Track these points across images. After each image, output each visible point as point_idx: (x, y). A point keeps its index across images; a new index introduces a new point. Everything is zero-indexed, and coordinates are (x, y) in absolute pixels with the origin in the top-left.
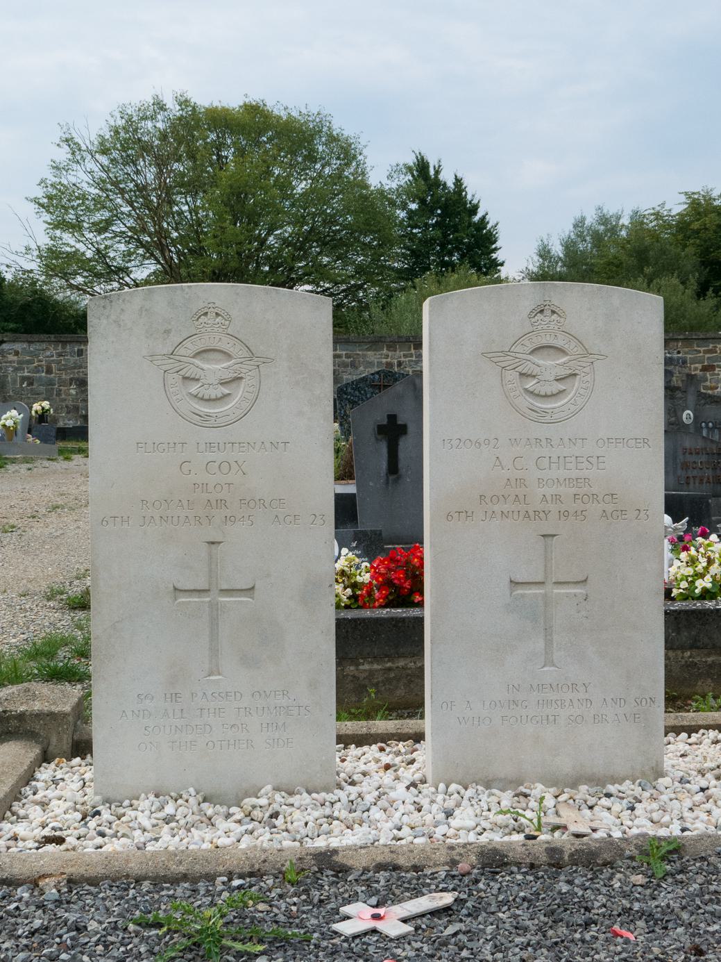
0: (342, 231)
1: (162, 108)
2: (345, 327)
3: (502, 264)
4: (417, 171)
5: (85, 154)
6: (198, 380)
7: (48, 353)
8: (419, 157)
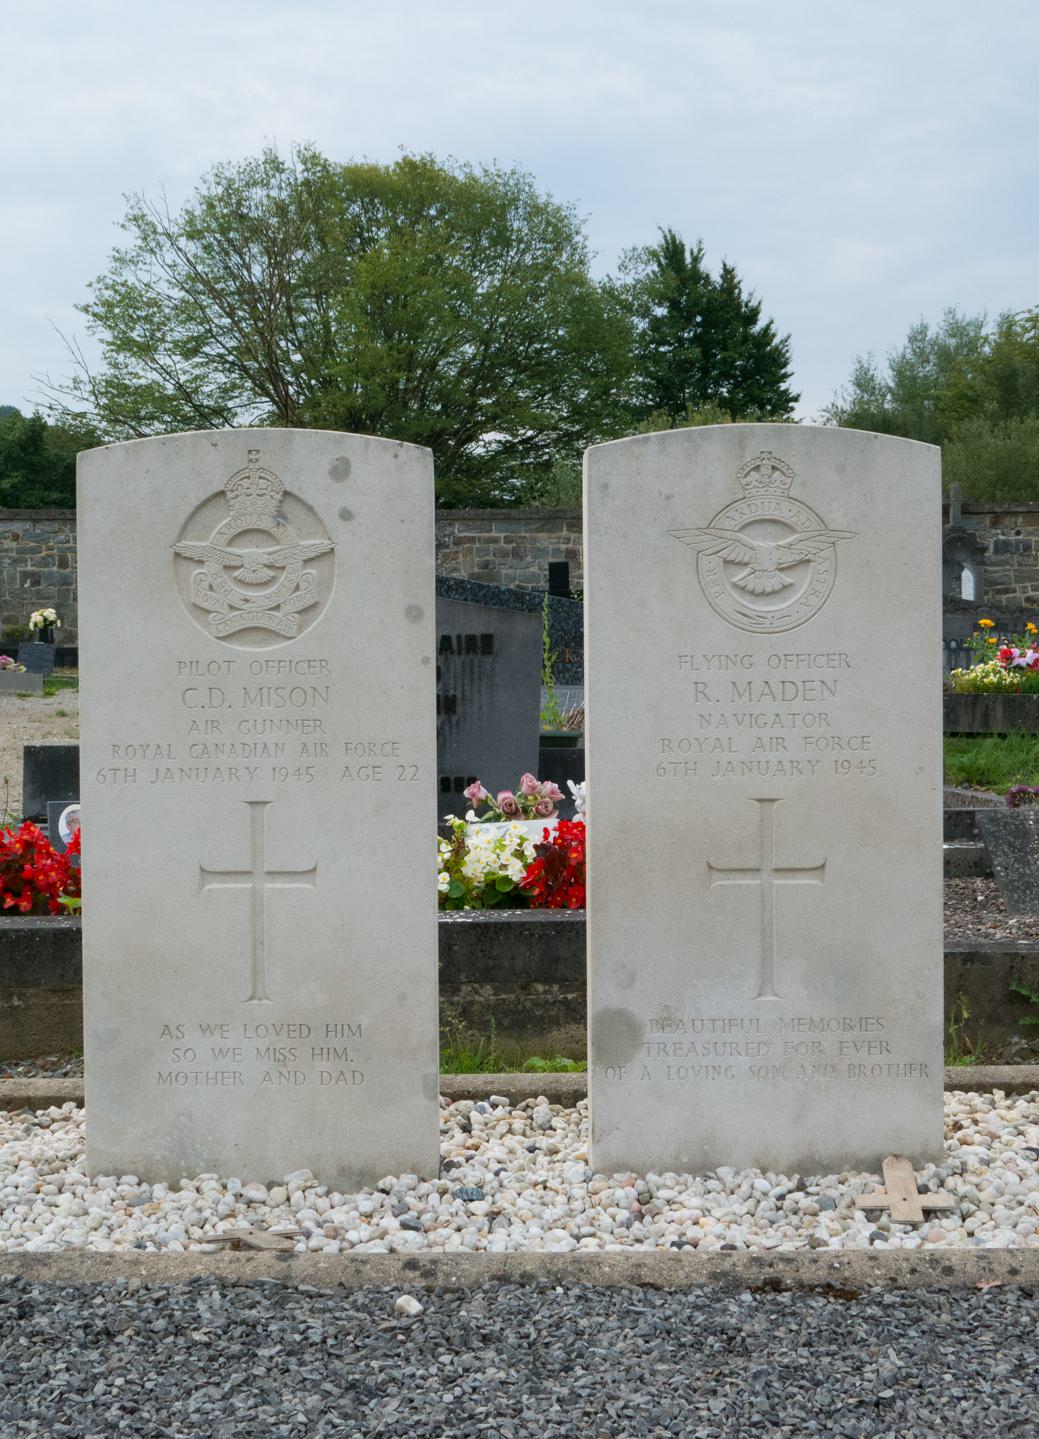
0: (551, 349)
2: (460, 493)
3: (796, 399)
4: (666, 258)
6: (746, 564)
7: (62, 537)
8: (669, 238)
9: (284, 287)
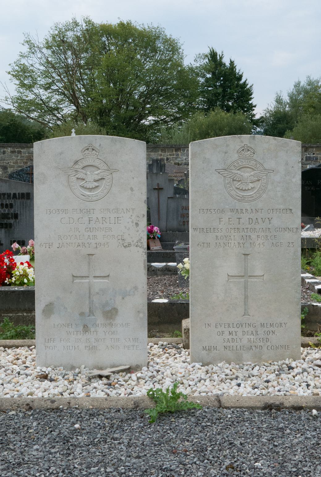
1: (77, 24)
3: (255, 106)
5: (36, 49)
9: (79, 66)
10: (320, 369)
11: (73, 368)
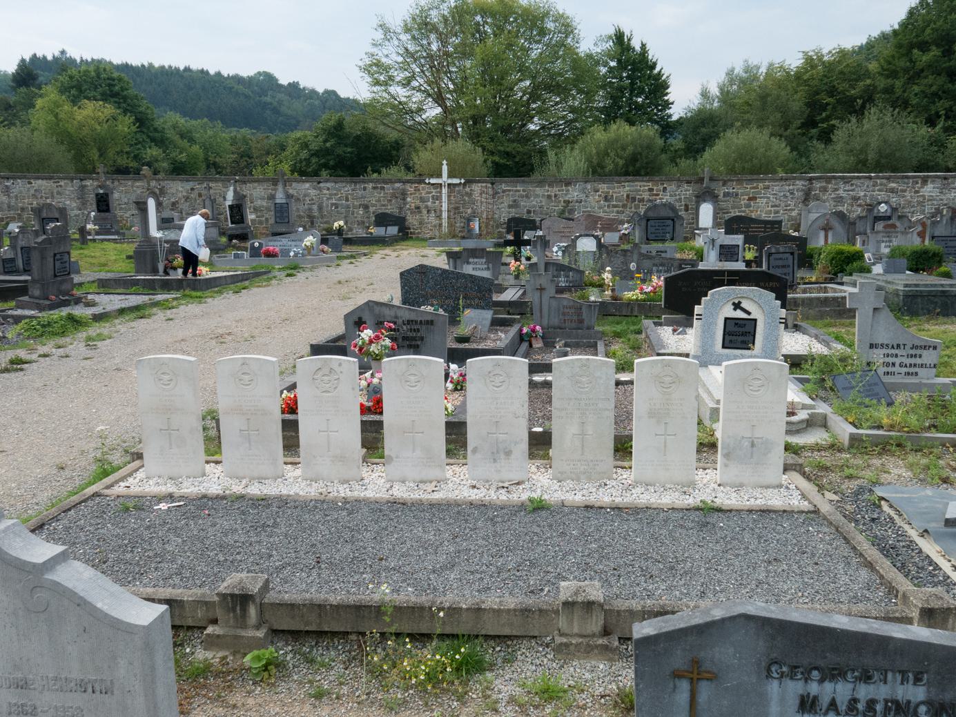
3: (672, 103)
9: (447, 54)
10: (943, 330)
11: (487, 481)
